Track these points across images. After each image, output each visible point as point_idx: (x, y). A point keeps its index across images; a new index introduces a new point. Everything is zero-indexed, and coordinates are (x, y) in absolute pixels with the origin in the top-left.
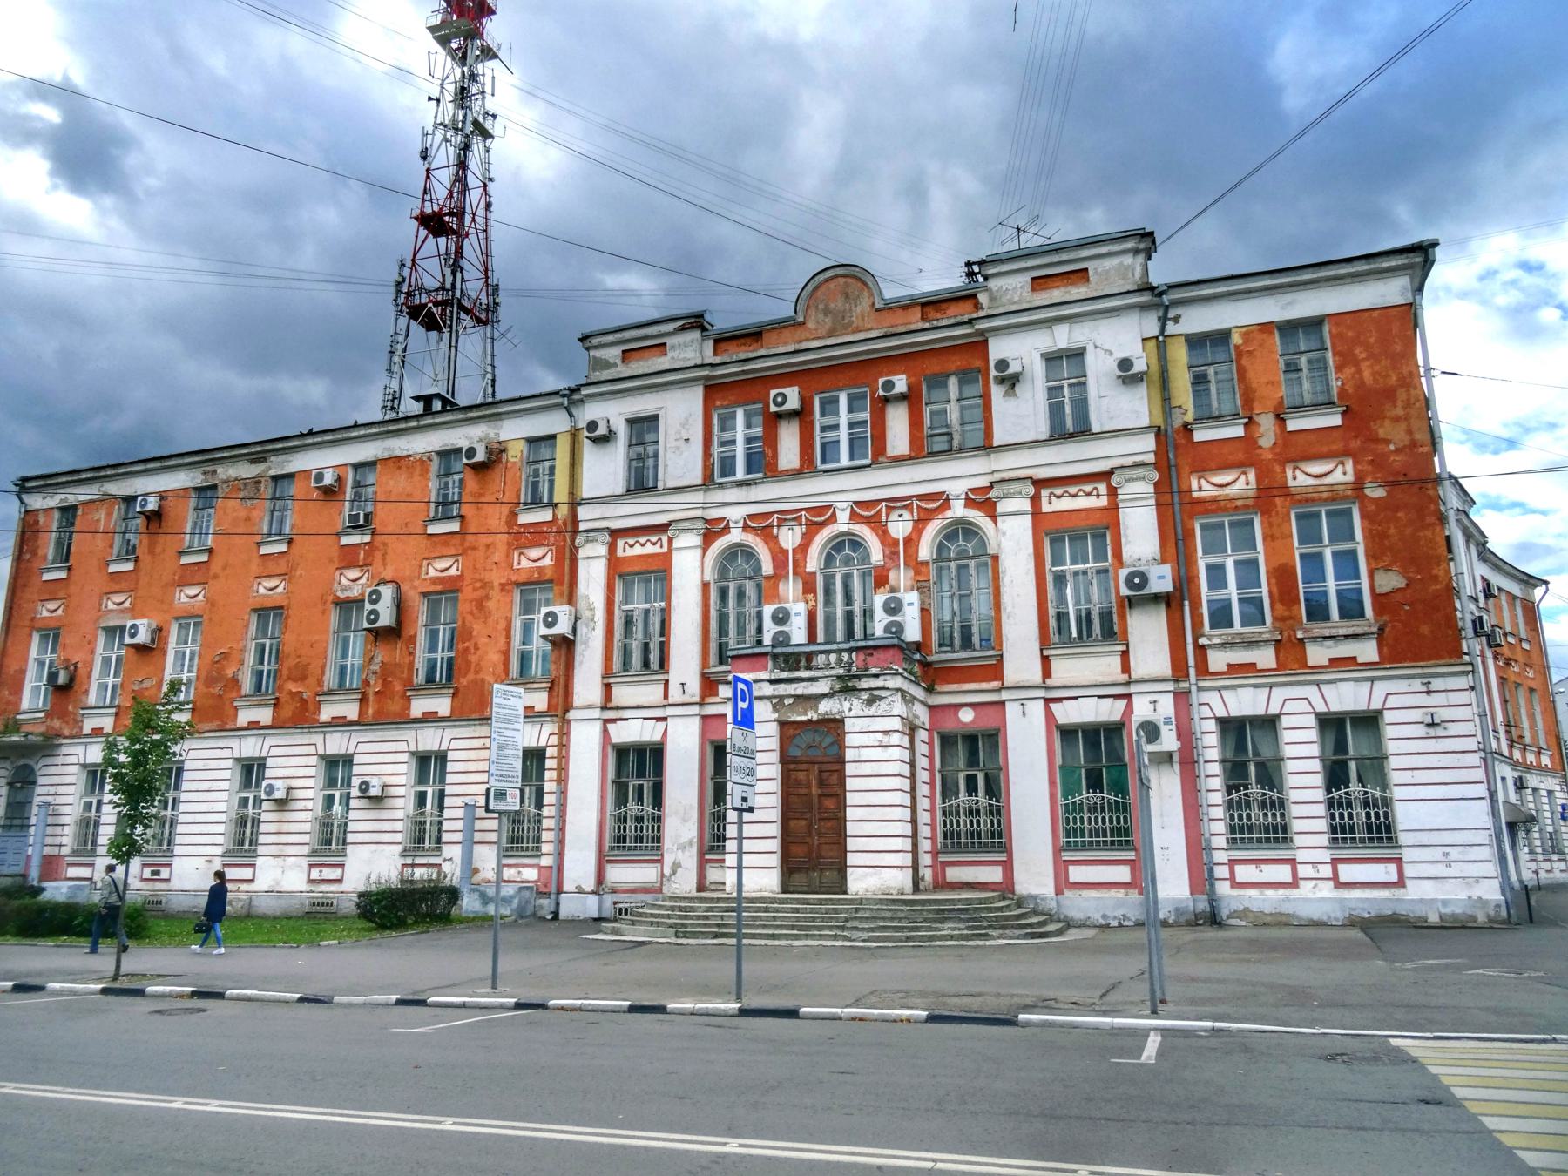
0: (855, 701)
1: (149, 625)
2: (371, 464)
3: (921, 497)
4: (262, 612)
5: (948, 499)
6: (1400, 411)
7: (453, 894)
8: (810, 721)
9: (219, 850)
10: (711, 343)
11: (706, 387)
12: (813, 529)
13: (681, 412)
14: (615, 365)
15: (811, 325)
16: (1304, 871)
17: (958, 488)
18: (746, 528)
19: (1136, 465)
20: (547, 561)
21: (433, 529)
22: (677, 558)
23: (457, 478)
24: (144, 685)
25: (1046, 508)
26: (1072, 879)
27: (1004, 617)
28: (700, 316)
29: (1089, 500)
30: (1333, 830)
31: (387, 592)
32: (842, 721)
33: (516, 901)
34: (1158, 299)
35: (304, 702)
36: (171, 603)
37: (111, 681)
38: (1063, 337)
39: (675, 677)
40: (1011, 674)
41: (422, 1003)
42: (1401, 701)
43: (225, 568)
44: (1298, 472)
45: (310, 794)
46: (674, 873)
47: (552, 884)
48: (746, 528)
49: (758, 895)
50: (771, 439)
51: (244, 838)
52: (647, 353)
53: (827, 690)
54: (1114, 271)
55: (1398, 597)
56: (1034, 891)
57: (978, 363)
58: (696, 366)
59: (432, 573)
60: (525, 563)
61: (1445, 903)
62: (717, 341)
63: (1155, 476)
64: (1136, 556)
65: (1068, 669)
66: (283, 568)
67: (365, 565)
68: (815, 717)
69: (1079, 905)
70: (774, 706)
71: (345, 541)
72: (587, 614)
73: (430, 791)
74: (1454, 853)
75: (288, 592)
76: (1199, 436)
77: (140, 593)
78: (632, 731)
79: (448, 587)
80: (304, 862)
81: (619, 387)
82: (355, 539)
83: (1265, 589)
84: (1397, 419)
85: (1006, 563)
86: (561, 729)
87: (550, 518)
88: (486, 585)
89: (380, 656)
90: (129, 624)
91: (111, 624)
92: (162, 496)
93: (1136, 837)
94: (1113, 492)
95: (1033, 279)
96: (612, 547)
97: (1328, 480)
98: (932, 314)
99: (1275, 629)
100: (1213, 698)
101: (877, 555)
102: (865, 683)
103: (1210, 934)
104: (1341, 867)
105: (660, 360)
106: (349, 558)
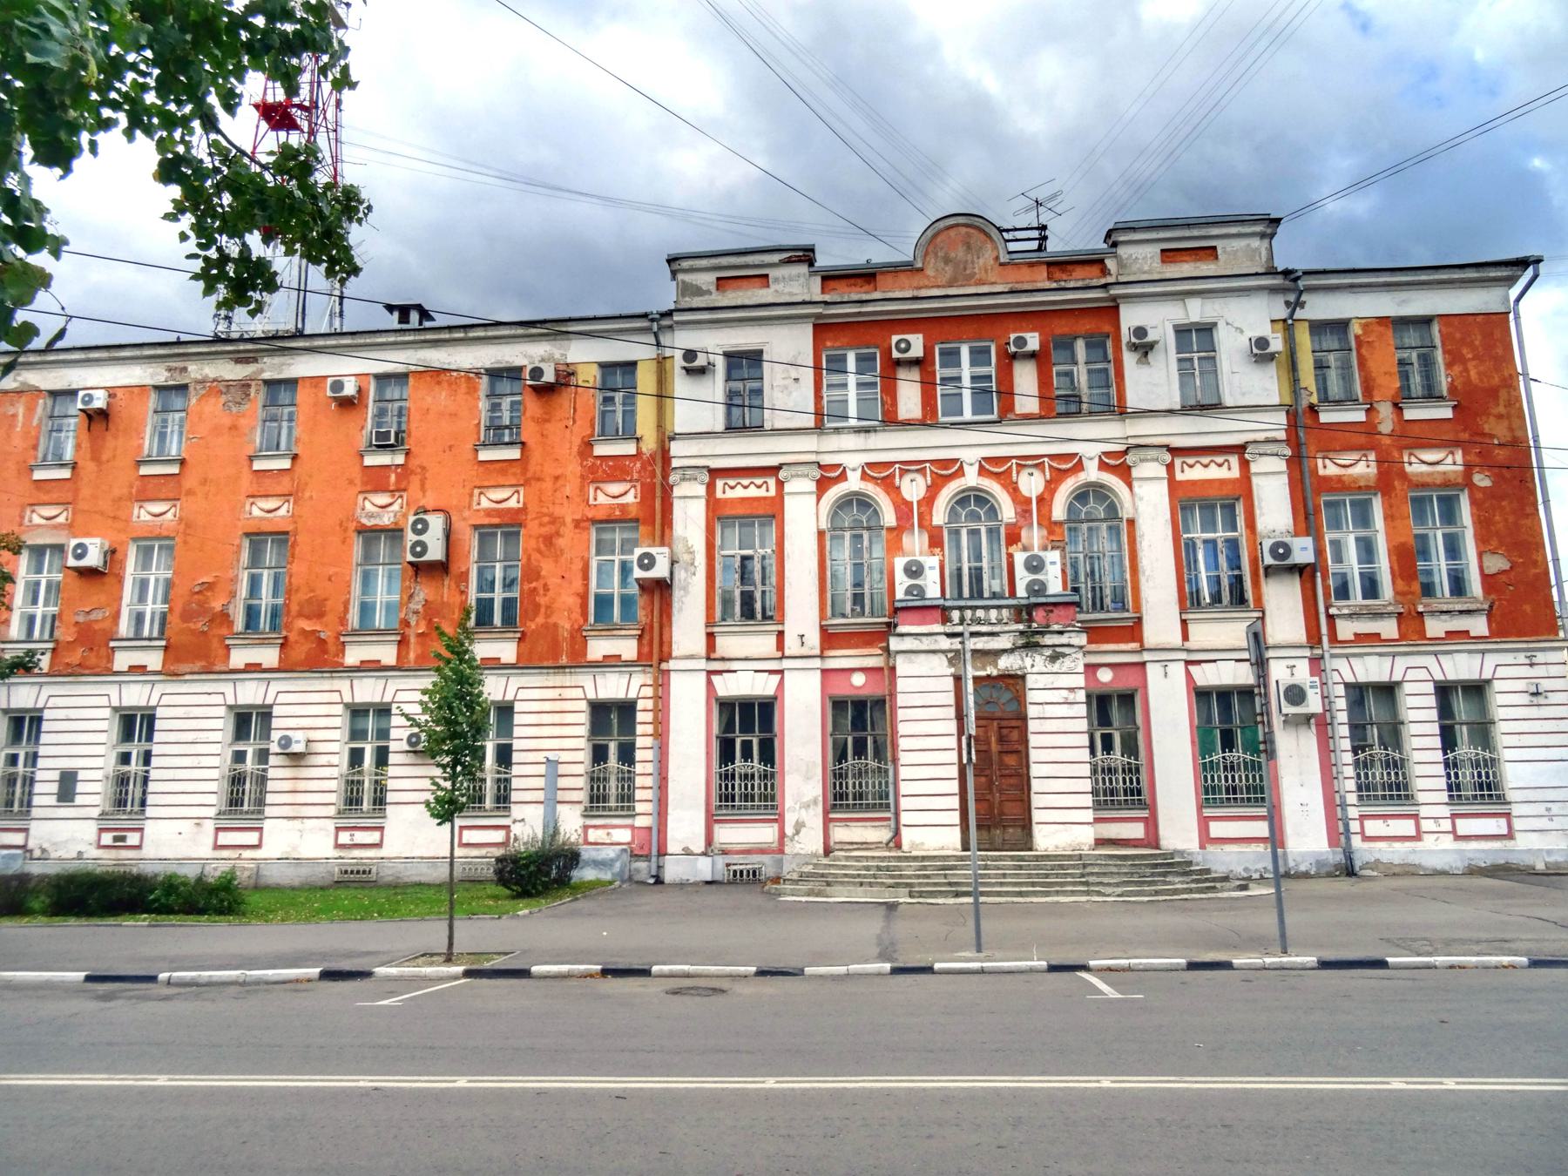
0: (1038, 658)
1: (102, 545)
2: (401, 378)
4: (257, 538)
5: (961, 467)
6: (1501, 409)
7: (572, 858)
8: (989, 676)
9: (212, 812)
10: (818, 280)
11: (815, 326)
12: (1057, 477)
13: (788, 348)
14: (709, 292)
15: (930, 272)
16: (1426, 825)
18: (865, 477)
19: (1268, 441)
20: (630, 498)
21: (484, 455)
22: (790, 504)
23: (177, 416)
24: (93, 616)
25: (1179, 477)
26: (1213, 835)
27: (1143, 580)
28: (810, 250)
29: (1224, 471)
30: (1450, 788)
31: (436, 523)
32: (1023, 677)
33: (618, 865)
34: (1291, 283)
35: (322, 642)
36: (128, 521)
37: (39, 611)
38: (1196, 311)
39: (791, 631)
40: (1151, 635)
41: (523, 973)
42: (1506, 672)
43: (204, 482)
44: (1413, 459)
45: (335, 747)
46: (797, 832)
47: (653, 845)
48: (865, 477)
50: (890, 390)
51: (242, 797)
52: (745, 283)
53: (1009, 646)
54: (1238, 253)
55: (1504, 578)
56: (1180, 846)
57: (1107, 328)
58: (804, 303)
59: (485, 504)
60: (602, 499)
61: (1549, 852)
62: (824, 279)
63: (1288, 452)
64: (1271, 527)
65: (728, 644)
66: (286, 485)
67: (399, 490)
68: (995, 673)
69: (1225, 860)
70: (950, 661)
71: (370, 460)
72: (686, 557)
73: (755, 742)
74: (1555, 808)
75: (294, 518)
76: (1325, 417)
77: (82, 505)
78: (743, 684)
79: (506, 520)
80: (330, 825)
81: (717, 316)
82: (383, 459)
84: (1500, 417)
85: (1143, 527)
86: (656, 679)
87: (633, 452)
88: (554, 520)
89: (423, 592)
90: (73, 542)
91: (40, 541)
92: (112, 392)
93: (1145, 796)
94: (1245, 465)
95: (718, 279)
96: (711, 487)
97: (1350, 471)
98: (1058, 275)
99: (1397, 602)
100: (1341, 664)
101: (1008, 512)
102: (1049, 640)
103: (1344, 885)
104: (1459, 822)
105: (764, 292)
106: (376, 480)
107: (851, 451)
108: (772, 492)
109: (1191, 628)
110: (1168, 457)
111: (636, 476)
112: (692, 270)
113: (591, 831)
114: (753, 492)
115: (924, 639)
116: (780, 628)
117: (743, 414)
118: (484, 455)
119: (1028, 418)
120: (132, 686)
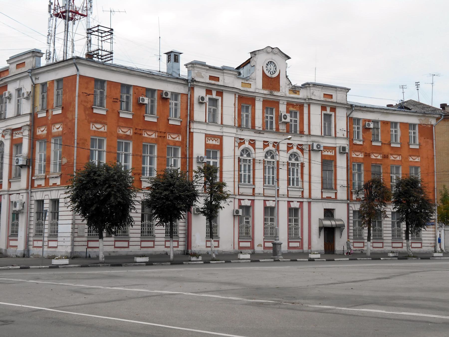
25: (14, 138)
108: (333, 154)
109: (323, 193)
120: (54, 191)
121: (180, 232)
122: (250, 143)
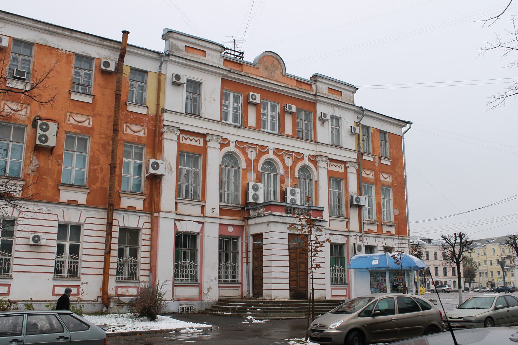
2: (29, 45)
3: (295, 153)
5: (268, 150)
17: (306, 153)
22: (209, 151)
46: (209, 291)
49: (282, 300)
52: (196, 51)
59: (72, 121)
65: (183, 208)
78: (189, 227)
81: (189, 64)
83: (22, 160)
84: (399, 167)
94: (205, 142)
105: (203, 58)
107: (235, 135)
109: (179, 206)
110: (178, 133)
111: (145, 124)
112: (177, 39)
113: (119, 289)
114: (193, 143)
115: (281, 218)
116: (204, 204)
117: (194, 110)
118: (74, 97)
119: (288, 136)
121: (142, 273)
122: (310, 160)
